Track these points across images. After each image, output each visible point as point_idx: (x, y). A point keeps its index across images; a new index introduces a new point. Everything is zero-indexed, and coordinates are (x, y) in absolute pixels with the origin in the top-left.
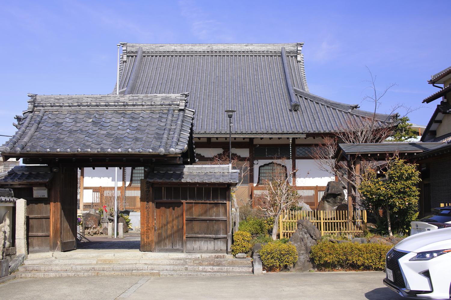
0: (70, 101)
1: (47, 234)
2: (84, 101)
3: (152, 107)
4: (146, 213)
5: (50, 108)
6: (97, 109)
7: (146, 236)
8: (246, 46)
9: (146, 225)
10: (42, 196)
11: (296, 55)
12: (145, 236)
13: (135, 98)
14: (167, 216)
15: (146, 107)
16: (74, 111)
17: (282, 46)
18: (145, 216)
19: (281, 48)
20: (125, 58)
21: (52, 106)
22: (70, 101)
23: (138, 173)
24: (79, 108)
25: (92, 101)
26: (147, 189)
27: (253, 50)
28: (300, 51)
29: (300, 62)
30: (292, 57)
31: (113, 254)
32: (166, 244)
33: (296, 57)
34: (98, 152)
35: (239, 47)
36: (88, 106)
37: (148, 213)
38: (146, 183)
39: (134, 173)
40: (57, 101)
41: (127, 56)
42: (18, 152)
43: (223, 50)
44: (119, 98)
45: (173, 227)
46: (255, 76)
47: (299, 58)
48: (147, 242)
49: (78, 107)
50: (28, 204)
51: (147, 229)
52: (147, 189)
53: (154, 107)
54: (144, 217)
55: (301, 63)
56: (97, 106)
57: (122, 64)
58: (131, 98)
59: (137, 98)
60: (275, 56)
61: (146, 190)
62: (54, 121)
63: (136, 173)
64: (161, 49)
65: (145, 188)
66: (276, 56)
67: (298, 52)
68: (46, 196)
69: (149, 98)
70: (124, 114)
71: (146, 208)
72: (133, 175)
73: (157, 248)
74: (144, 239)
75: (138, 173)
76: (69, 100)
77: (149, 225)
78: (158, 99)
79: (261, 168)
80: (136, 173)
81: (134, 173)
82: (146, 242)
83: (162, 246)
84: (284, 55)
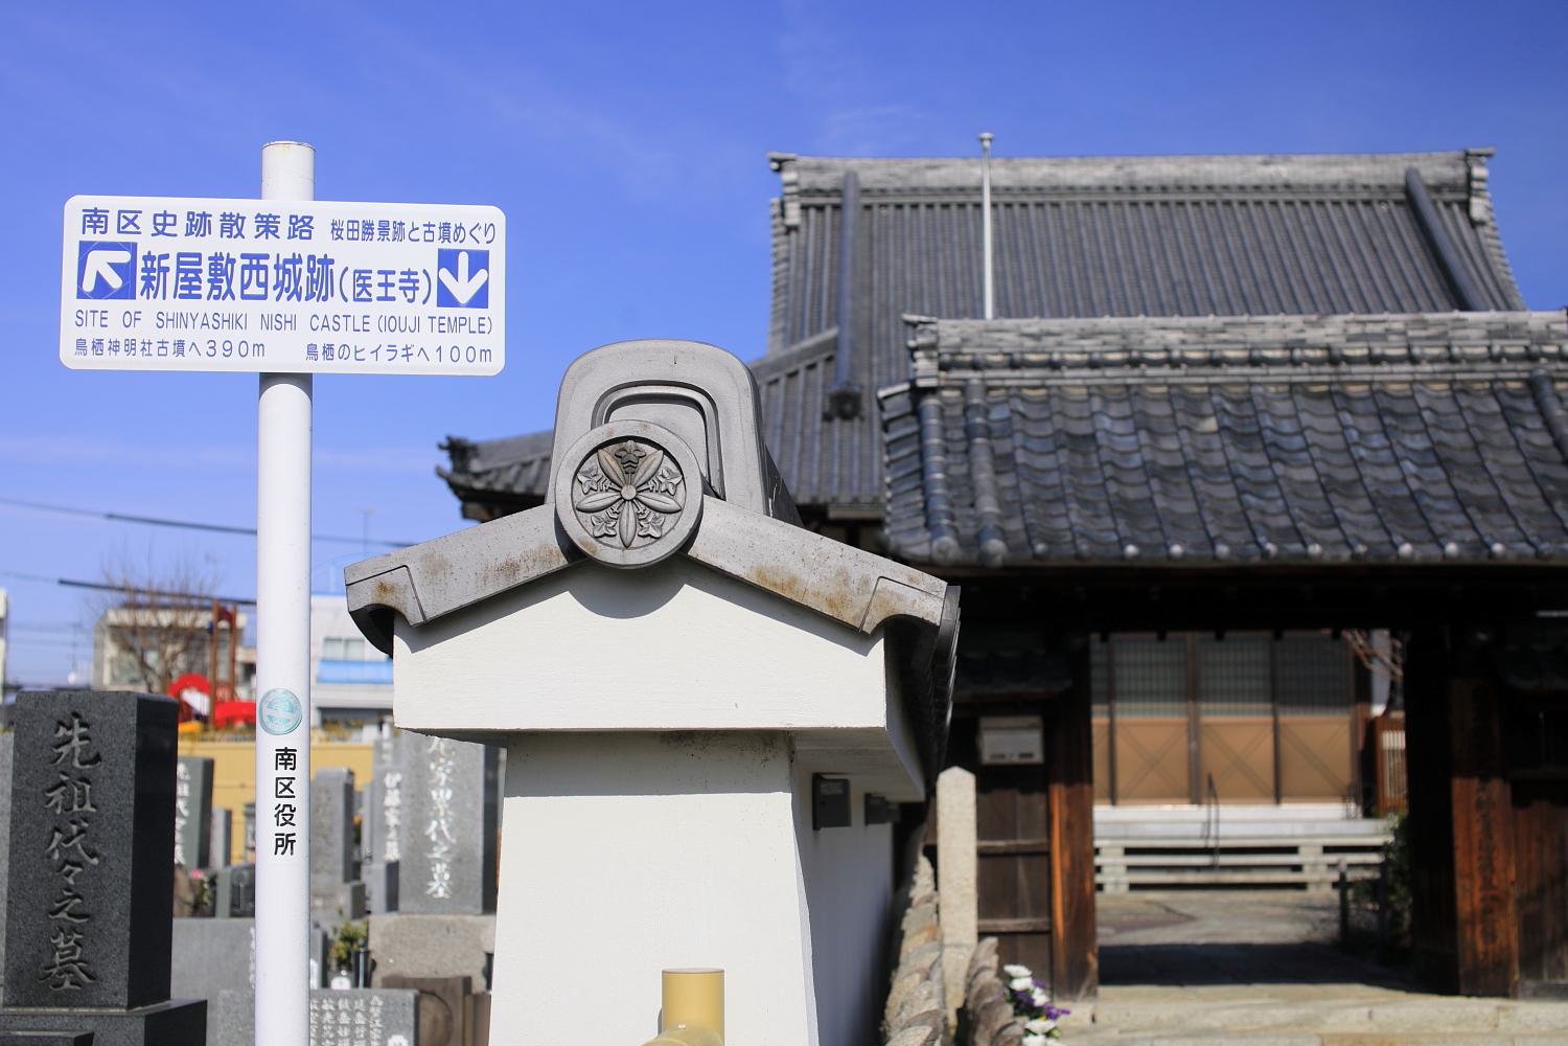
0: (1088, 344)
1: (1038, 922)
2: (1149, 343)
3: (1456, 367)
5: (1007, 373)
6: (1217, 376)
7: (1484, 931)
8: (1266, 163)
9: (1478, 882)
10: (1022, 756)
11: (1463, 196)
12: (1479, 928)
13: (1370, 328)
15: (1428, 368)
16: (1116, 386)
17: (1407, 164)
19: (1401, 172)
20: (794, 215)
21: (1013, 365)
22: (1088, 344)
24: (1136, 372)
25: (1183, 342)
27: (1293, 181)
28: (1481, 180)
29: (1482, 223)
30: (1448, 205)
31: (1365, 1010)
33: (1466, 206)
34: (1355, 556)
35: (1238, 168)
36: (1174, 363)
37: (1487, 829)
40: (1029, 343)
41: (805, 208)
42: (998, 561)
43: (1177, 180)
44: (1302, 331)
46: (960, 299)
47: (1478, 208)
48: (1486, 953)
49: (1127, 371)
50: (982, 788)
53: (1464, 366)
55: (1487, 230)
56: (1215, 362)
57: (783, 238)
58: (1355, 329)
59: (1379, 329)
60: (1380, 202)
62: (1048, 429)
64: (933, 178)
66: (1386, 202)
67: (1475, 185)
68: (1038, 758)
69: (1432, 332)
70: (1336, 397)
73: (1530, 984)
76: (1082, 337)
78: (1473, 333)
83: (1545, 974)
84: (1424, 199)
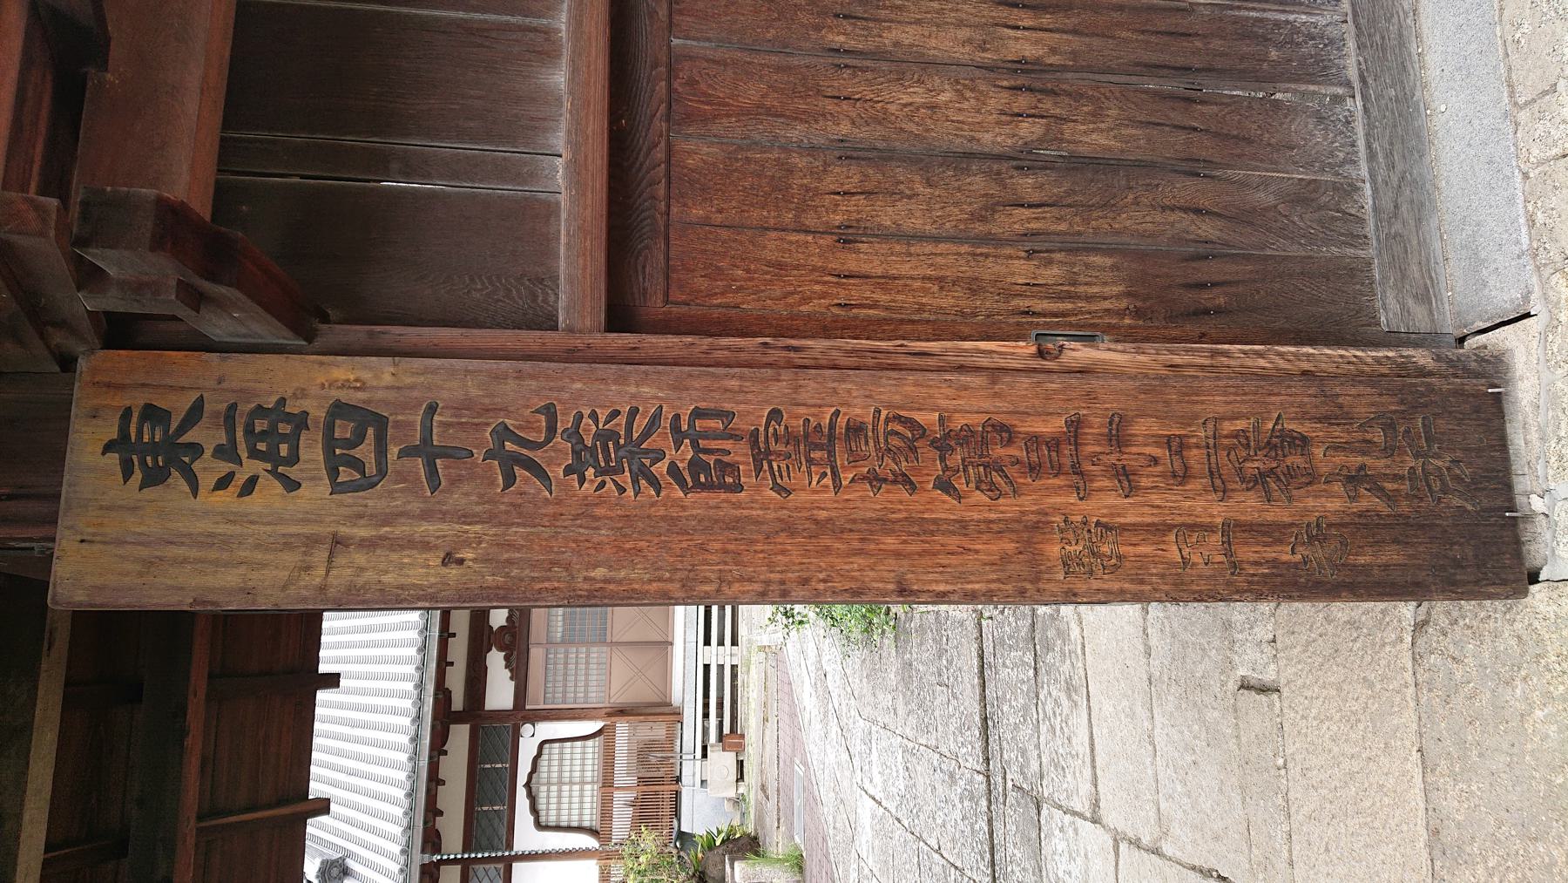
4: (813, 492)
9: (1052, 497)
14: (848, 153)
18: (870, 502)
23: (559, 809)
26: (312, 452)
32: (1304, 196)
37: (822, 443)
38: (154, 478)
39: (581, 820)
45: (1021, 66)
51: (1126, 478)
52: (312, 452)
54: (884, 524)
61: (315, 492)
63: (559, 815)
65: (270, 494)
71: (708, 474)
72: (564, 824)
74: (1317, 533)
75: (559, 809)
77: (1053, 426)
79: (552, 820)
80: (559, 815)
81: (581, 820)
82: (1368, 501)
